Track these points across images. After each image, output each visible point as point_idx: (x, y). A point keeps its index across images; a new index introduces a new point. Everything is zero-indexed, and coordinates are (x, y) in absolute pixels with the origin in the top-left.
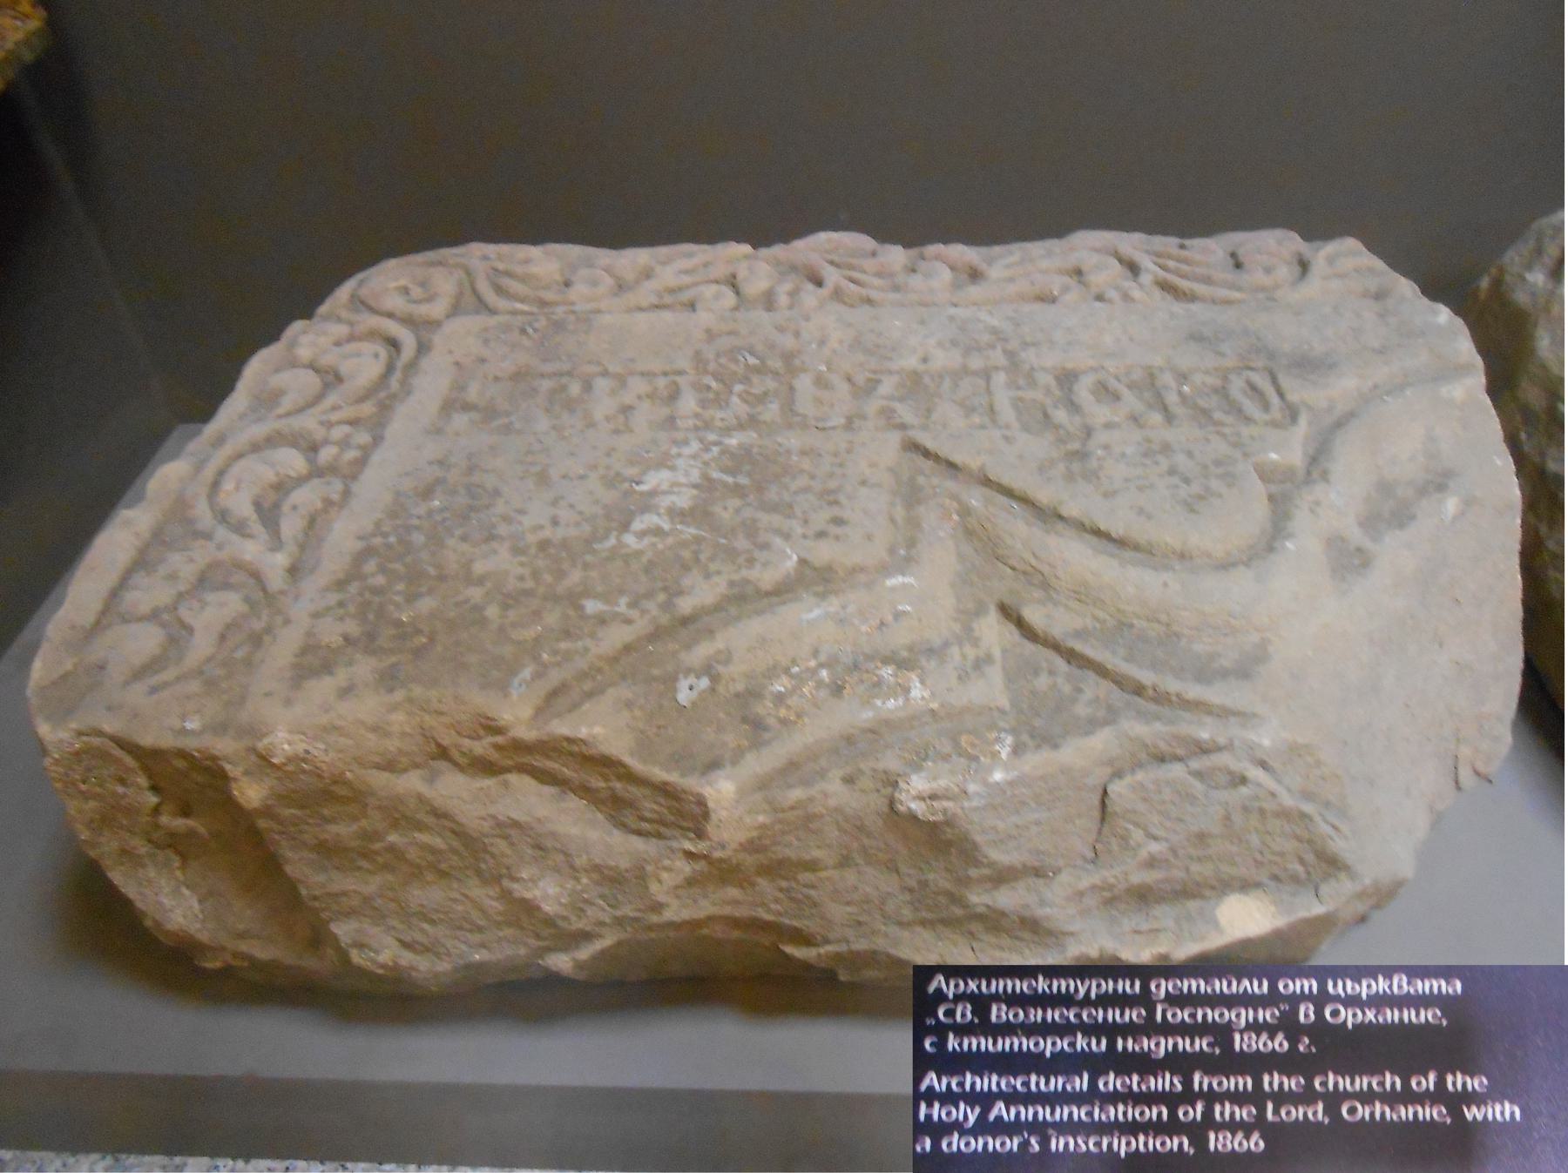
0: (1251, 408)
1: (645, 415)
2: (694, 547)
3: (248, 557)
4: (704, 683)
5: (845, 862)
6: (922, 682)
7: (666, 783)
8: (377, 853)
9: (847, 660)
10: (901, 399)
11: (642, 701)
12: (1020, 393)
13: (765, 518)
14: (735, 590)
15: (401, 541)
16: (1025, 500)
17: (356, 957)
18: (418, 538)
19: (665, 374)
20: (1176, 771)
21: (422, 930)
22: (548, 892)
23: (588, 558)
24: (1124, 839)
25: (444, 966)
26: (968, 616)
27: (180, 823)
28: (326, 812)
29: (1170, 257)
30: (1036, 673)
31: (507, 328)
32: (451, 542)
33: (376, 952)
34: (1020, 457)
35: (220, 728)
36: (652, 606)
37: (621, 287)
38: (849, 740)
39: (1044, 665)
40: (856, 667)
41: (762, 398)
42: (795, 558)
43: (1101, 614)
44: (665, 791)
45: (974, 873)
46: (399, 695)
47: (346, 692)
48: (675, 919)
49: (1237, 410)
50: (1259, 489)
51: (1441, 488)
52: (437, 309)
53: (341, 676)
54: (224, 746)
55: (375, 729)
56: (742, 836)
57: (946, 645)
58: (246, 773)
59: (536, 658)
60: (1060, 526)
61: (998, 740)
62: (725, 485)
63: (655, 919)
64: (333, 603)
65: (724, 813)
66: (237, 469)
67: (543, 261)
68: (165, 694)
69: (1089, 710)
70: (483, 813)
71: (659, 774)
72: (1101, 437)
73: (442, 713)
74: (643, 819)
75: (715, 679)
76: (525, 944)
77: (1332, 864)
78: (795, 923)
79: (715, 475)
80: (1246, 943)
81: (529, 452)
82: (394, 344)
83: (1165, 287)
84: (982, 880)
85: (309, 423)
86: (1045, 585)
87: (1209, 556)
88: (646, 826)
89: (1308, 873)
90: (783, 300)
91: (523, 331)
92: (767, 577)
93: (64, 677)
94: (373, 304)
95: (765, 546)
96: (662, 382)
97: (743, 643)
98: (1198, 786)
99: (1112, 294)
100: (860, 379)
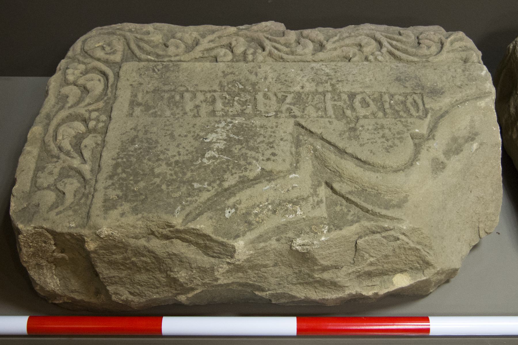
0: (413, 111)
1: (204, 109)
2: (227, 164)
3: (75, 166)
4: (233, 210)
5: (276, 265)
6: (301, 209)
7: (222, 242)
8: (127, 264)
9: (277, 202)
10: (294, 104)
11: (215, 217)
12: (335, 103)
13: (250, 153)
14: (241, 179)
15: (128, 161)
16: (334, 146)
17: (114, 298)
18: (134, 159)
19: (210, 92)
20: (378, 236)
21: (138, 289)
22: (182, 275)
23: (192, 167)
24: (363, 257)
25: (143, 300)
26: (315, 187)
27: (60, 255)
28: (113, 251)
29: (394, 39)
30: (336, 205)
31: (147, 69)
32: (145, 161)
33: (121, 296)
34: (333, 129)
35: (83, 226)
36: (215, 185)
37: (189, 49)
38: (278, 228)
39: (339, 202)
40: (280, 204)
41: (245, 103)
42: (260, 168)
43: (357, 187)
44: (222, 244)
45: (316, 268)
46: (140, 216)
47: (122, 215)
48: (222, 283)
49: (407, 111)
50: (410, 142)
51: (473, 139)
52: (117, 57)
53: (120, 210)
54: (85, 232)
55: (132, 226)
56: (245, 257)
57: (308, 197)
58: (91, 240)
59: (181, 203)
60: (346, 156)
61: (323, 227)
62: (235, 139)
63: (215, 283)
64: (110, 184)
65: (240, 250)
66: (61, 130)
67: (155, 32)
68: (62, 215)
69: (352, 218)
70: (164, 251)
71: (221, 239)
72: (361, 122)
73: (153, 221)
74: (214, 252)
75: (237, 209)
76: (172, 292)
77: (428, 264)
78: (259, 284)
79: (232, 135)
80: (402, 289)
81: (165, 125)
82: (104, 74)
83: (391, 53)
84: (318, 270)
85: (81, 110)
86: (340, 176)
87: (392, 167)
88: (215, 254)
89: (421, 267)
90: (250, 57)
91: (154, 70)
92: (251, 175)
93: (24, 209)
94: (91, 54)
95: (250, 164)
96: (209, 95)
97: (244, 197)
98: (385, 241)
99: (371, 58)
100: (280, 95)
